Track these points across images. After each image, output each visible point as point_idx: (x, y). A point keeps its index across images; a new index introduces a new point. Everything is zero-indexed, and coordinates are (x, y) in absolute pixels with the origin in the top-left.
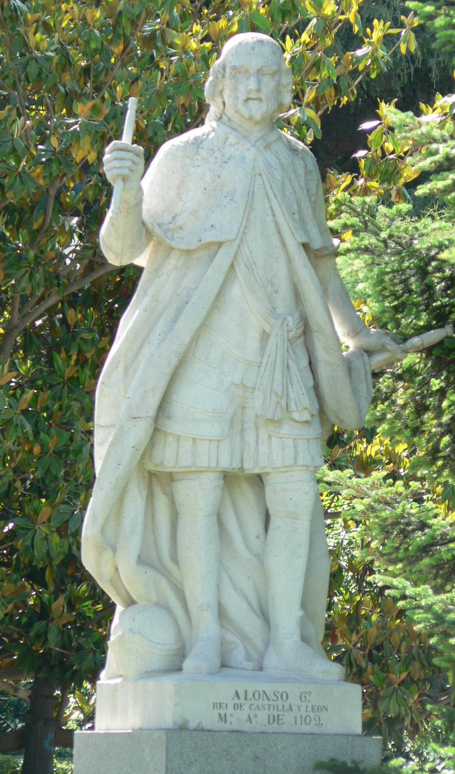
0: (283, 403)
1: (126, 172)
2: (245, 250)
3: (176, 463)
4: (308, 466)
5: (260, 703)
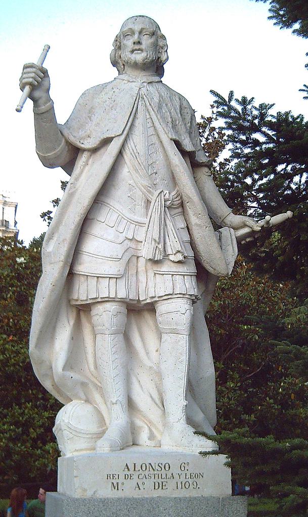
0: (161, 246)
3: (173, 292)
5: (147, 473)
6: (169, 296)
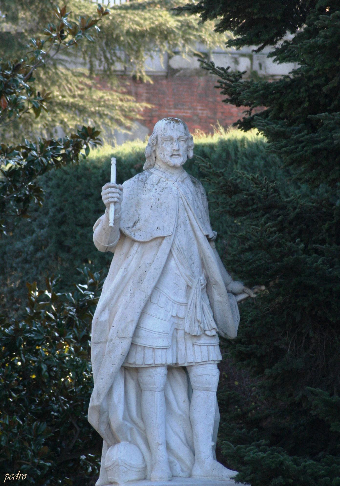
1: (116, 199)
2: (177, 241)
4: (214, 361)
6: (204, 363)
